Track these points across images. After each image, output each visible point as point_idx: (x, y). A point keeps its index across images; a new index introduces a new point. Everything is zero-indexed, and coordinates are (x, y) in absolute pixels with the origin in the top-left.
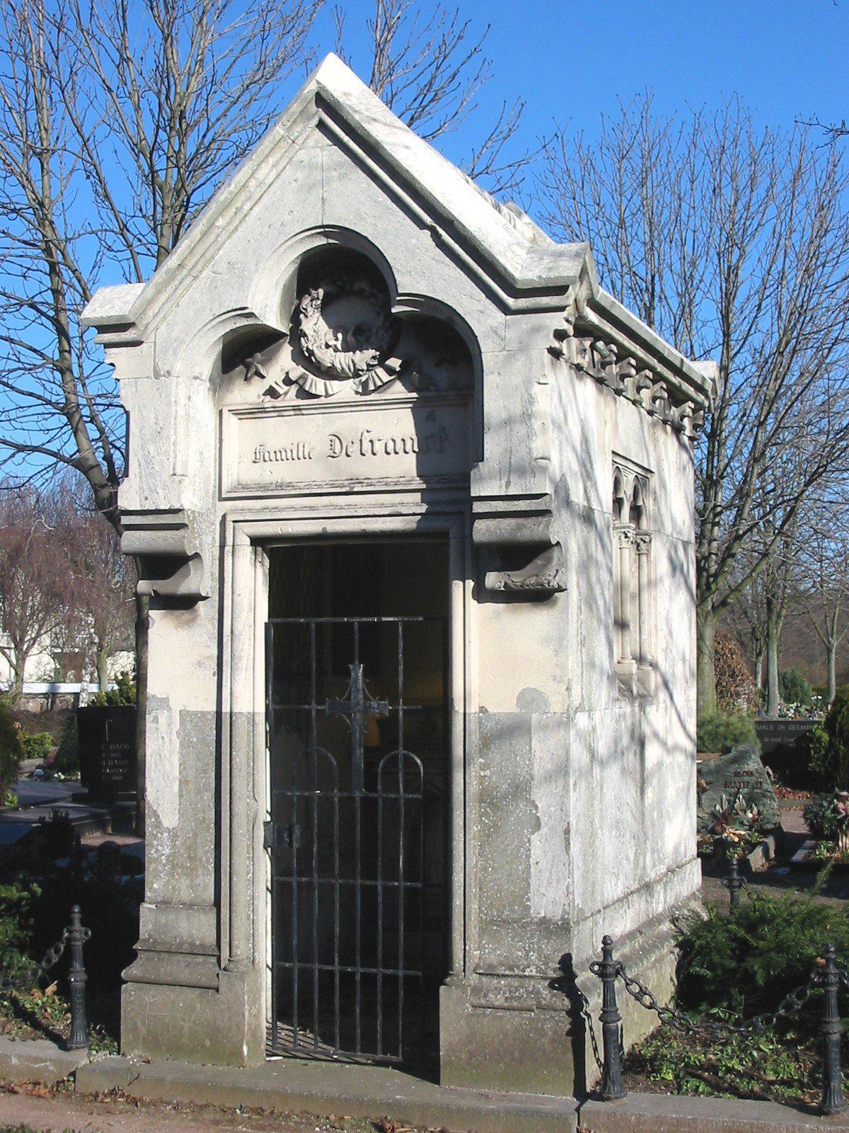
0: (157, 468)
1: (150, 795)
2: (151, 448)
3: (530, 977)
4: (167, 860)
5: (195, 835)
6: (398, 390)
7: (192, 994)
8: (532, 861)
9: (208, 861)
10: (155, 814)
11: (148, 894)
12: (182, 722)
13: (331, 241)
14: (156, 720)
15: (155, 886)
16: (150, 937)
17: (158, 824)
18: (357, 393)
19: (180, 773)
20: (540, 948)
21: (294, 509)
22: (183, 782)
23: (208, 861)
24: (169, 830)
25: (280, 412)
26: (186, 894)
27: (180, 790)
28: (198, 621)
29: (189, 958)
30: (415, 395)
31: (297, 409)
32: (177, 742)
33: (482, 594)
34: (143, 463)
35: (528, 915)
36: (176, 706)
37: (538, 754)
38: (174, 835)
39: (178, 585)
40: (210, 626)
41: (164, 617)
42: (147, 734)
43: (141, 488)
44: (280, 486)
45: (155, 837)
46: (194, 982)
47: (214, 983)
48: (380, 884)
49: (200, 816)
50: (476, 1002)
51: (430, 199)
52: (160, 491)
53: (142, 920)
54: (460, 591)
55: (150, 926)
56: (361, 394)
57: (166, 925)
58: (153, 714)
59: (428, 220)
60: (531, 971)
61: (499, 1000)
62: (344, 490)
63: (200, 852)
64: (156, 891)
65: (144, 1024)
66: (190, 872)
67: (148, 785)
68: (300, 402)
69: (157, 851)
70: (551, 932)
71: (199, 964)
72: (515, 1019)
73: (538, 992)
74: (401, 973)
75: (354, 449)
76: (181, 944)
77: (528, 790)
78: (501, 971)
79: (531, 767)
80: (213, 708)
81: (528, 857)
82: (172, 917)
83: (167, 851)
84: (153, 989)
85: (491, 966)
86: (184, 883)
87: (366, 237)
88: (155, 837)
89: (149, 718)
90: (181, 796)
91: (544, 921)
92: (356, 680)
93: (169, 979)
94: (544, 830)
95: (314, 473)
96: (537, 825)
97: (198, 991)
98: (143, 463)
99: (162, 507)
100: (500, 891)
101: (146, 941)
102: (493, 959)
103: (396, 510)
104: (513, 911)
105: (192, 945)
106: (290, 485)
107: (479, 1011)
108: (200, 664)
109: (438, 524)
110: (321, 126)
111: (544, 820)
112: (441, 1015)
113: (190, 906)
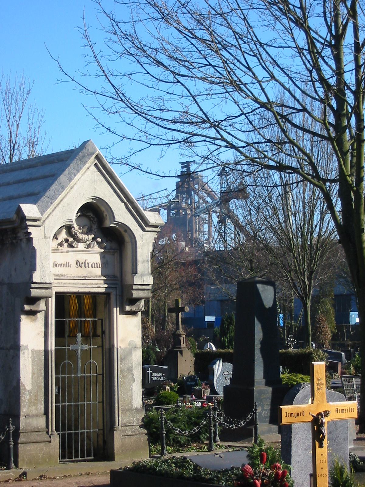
0: (46, 269)
1: (22, 379)
2: (44, 262)
3: (135, 425)
4: (28, 401)
5: (37, 391)
6: (97, 248)
7: (42, 445)
8: (133, 391)
9: (41, 400)
10: (24, 385)
11: (22, 413)
12: (33, 354)
13: (93, 201)
14: (24, 353)
15: (24, 410)
16: (24, 427)
17: (25, 389)
18: (85, 247)
19: (32, 371)
20: (136, 417)
21: (92, 284)
22: (33, 374)
23: (41, 400)
24: (28, 391)
25: (62, 251)
26: (34, 412)
27: (32, 377)
28: (38, 320)
29: (37, 433)
30: (103, 250)
31: (68, 251)
32: (31, 361)
33: (123, 312)
34: (41, 267)
35: (132, 407)
36: (30, 348)
37: (134, 360)
38: (30, 392)
39: (39, 307)
40: (41, 321)
41: (27, 318)
42: (21, 359)
43: (41, 275)
44: (62, 276)
45: (24, 393)
46: (43, 440)
47: (49, 440)
48: (85, 403)
49: (39, 385)
50: (123, 434)
51: (128, 195)
52: (47, 277)
53: (21, 422)
54: (116, 311)
55: (24, 424)
56: (87, 248)
57: (29, 423)
58: (23, 351)
59: (125, 201)
60: (135, 424)
61: (129, 433)
62: (83, 278)
63: (39, 398)
64: (24, 412)
65: (26, 457)
66: (35, 404)
67: (21, 376)
68: (68, 249)
69: (24, 398)
70: (139, 412)
71: (41, 435)
72: (134, 438)
73: (138, 430)
74: (92, 430)
75: (83, 265)
76: (35, 428)
77: (132, 371)
78: (128, 424)
79: (132, 363)
80: (42, 348)
81: (132, 390)
82: (31, 420)
83: (28, 398)
84: (29, 445)
85: (124, 424)
86: (33, 408)
87: (106, 203)
88: (24, 393)
89: (21, 353)
90: (32, 379)
91: (136, 409)
92: (79, 339)
93: (35, 441)
94: (136, 382)
95: (74, 271)
96: (134, 380)
97: (44, 443)
98: (41, 267)
99: (47, 282)
100: (125, 401)
101: (22, 429)
102: (125, 422)
103: (98, 285)
104: (128, 406)
105: (38, 428)
106: (65, 276)
107: (124, 437)
108: (38, 334)
109: (110, 290)
110: (96, 165)
111: (136, 379)
112: (115, 439)
113: (37, 416)
